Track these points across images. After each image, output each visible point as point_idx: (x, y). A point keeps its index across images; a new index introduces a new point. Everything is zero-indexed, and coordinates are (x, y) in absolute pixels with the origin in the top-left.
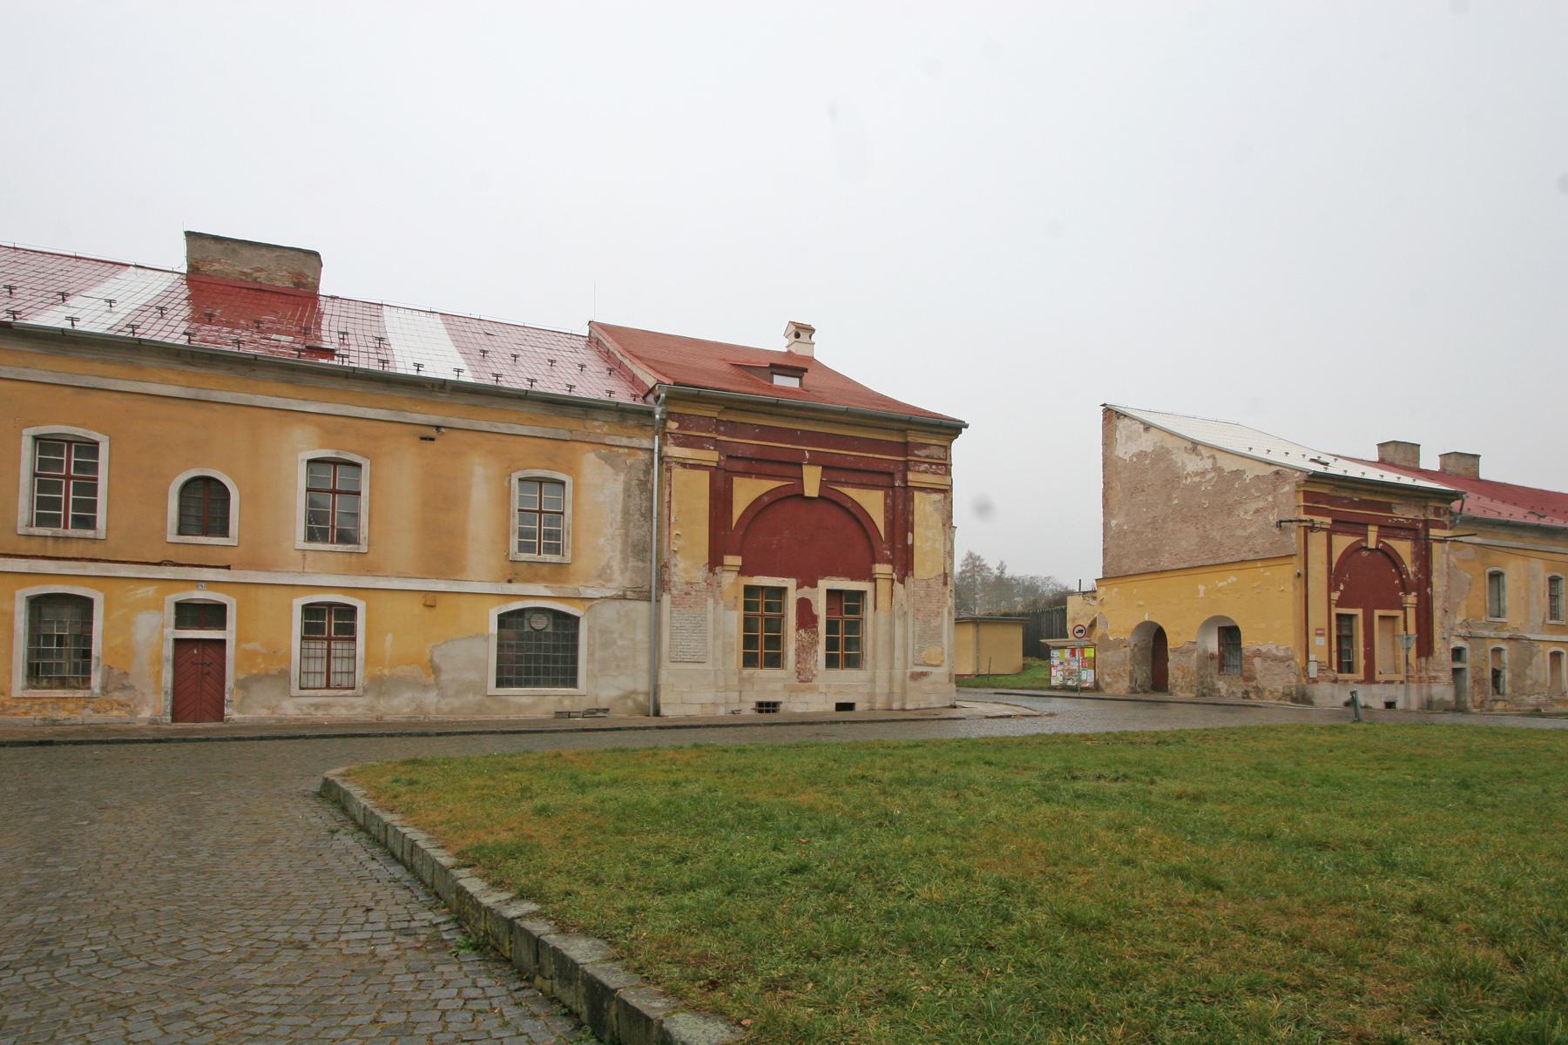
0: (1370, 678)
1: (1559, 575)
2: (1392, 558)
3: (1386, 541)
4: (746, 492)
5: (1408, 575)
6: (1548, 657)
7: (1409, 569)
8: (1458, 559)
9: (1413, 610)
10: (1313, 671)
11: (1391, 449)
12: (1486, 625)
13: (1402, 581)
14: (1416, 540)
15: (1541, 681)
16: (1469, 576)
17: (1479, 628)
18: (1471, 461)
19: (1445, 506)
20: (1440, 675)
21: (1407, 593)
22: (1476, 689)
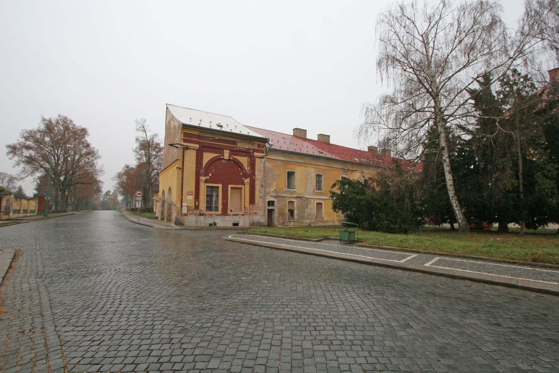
0: (225, 212)
1: (321, 174)
2: (239, 165)
3: (235, 157)
4: (208, 157)
5: (246, 171)
6: (315, 204)
7: (246, 168)
8: (272, 166)
9: (249, 185)
10: (185, 211)
11: (296, 130)
12: (286, 192)
13: (243, 173)
14: (250, 157)
15: (312, 214)
16: (278, 172)
17: (282, 193)
18: (327, 137)
19: (263, 144)
20: (258, 212)
21: (246, 178)
22: (280, 217)
